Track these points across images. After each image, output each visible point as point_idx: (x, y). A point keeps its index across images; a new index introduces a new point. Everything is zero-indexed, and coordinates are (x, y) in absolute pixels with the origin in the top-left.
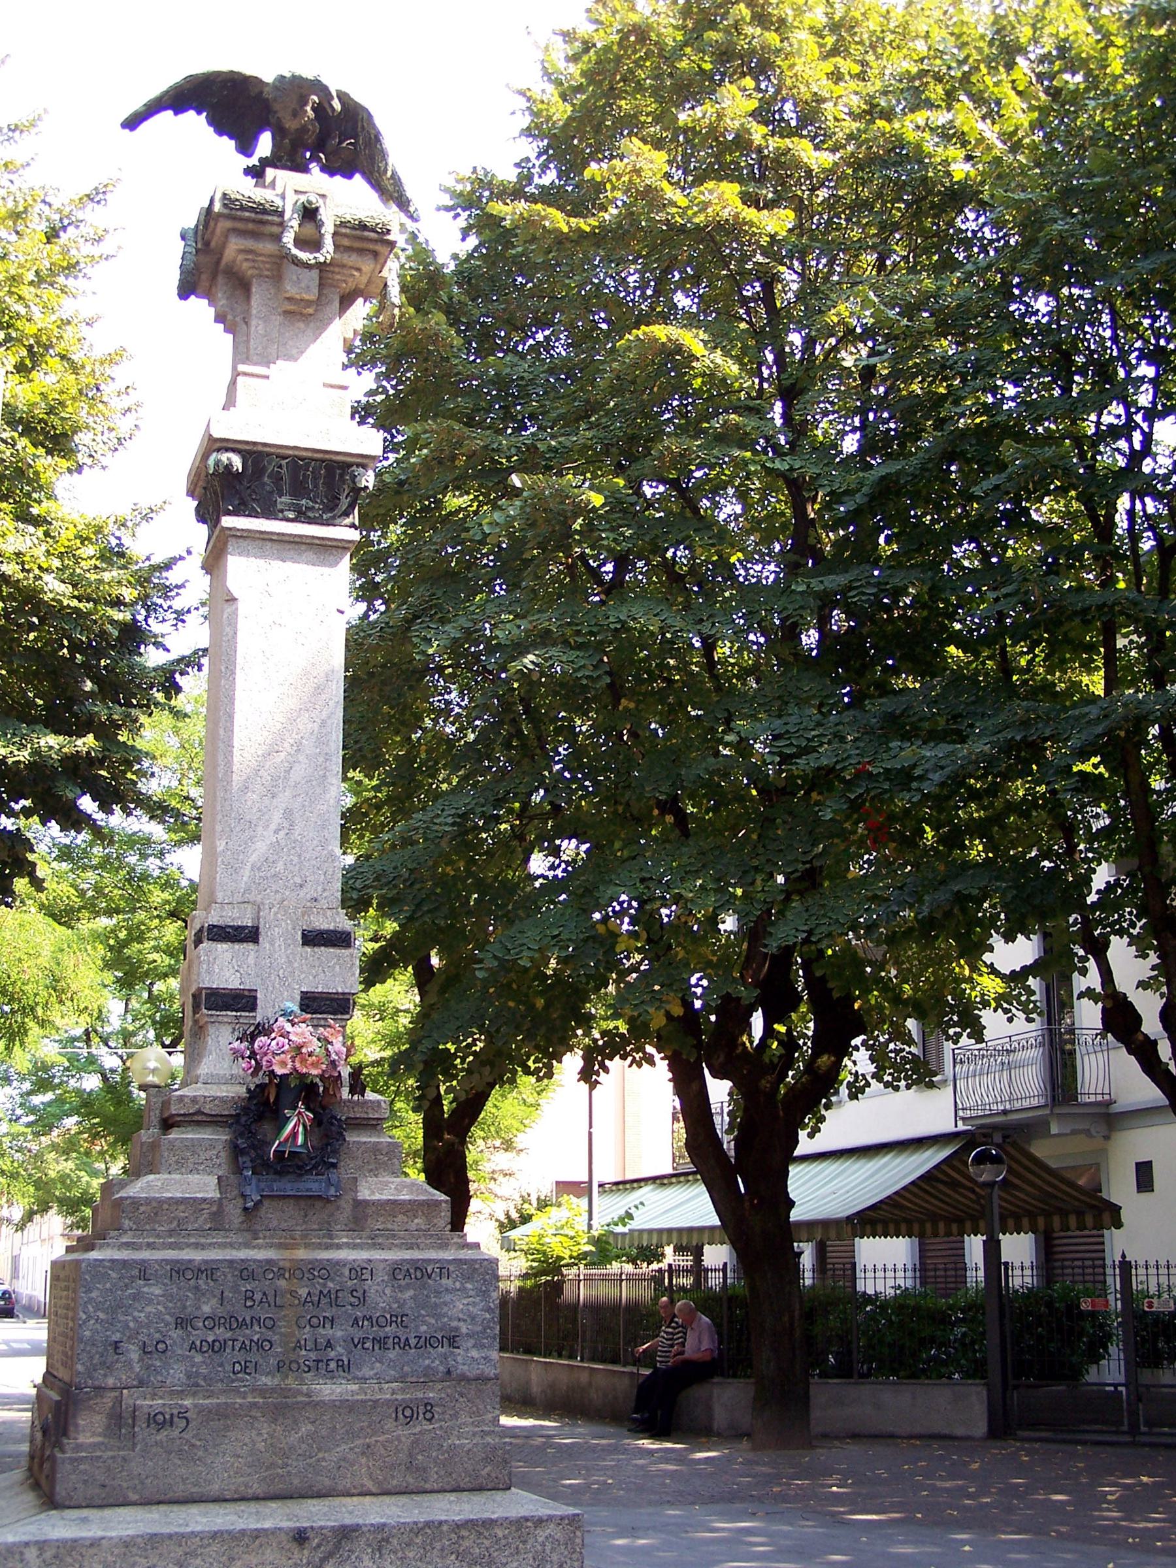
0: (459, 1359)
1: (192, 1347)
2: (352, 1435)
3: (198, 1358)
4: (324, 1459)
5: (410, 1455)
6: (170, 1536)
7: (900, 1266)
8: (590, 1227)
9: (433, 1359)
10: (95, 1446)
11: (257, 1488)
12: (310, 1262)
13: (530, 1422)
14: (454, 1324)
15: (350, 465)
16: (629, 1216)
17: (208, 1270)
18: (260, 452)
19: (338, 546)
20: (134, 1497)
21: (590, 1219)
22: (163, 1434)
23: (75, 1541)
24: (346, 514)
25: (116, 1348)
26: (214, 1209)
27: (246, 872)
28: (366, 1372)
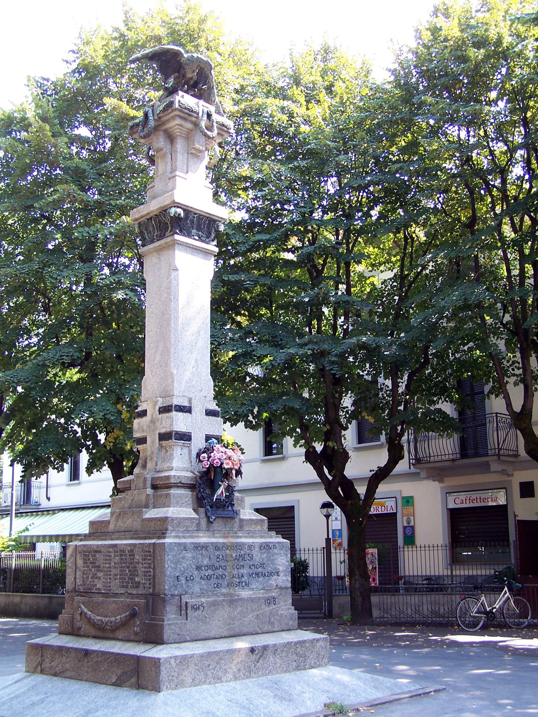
1: (201, 578)
2: (253, 611)
3: (203, 582)
6: (214, 652)
7: (440, 545)
10: (174, 618)
11: (225, 633)
12: (236, 543)
13: (8, 619)
14: (278, 567)
15: (216, 221)
16: (27, 529)
17: (205, 547)
18: (189, 210)
20: (188, 639)
21: (11, 530)
23: (186, 656)
24: (213, 241)
27: (184, 384)
28: (254, 586)
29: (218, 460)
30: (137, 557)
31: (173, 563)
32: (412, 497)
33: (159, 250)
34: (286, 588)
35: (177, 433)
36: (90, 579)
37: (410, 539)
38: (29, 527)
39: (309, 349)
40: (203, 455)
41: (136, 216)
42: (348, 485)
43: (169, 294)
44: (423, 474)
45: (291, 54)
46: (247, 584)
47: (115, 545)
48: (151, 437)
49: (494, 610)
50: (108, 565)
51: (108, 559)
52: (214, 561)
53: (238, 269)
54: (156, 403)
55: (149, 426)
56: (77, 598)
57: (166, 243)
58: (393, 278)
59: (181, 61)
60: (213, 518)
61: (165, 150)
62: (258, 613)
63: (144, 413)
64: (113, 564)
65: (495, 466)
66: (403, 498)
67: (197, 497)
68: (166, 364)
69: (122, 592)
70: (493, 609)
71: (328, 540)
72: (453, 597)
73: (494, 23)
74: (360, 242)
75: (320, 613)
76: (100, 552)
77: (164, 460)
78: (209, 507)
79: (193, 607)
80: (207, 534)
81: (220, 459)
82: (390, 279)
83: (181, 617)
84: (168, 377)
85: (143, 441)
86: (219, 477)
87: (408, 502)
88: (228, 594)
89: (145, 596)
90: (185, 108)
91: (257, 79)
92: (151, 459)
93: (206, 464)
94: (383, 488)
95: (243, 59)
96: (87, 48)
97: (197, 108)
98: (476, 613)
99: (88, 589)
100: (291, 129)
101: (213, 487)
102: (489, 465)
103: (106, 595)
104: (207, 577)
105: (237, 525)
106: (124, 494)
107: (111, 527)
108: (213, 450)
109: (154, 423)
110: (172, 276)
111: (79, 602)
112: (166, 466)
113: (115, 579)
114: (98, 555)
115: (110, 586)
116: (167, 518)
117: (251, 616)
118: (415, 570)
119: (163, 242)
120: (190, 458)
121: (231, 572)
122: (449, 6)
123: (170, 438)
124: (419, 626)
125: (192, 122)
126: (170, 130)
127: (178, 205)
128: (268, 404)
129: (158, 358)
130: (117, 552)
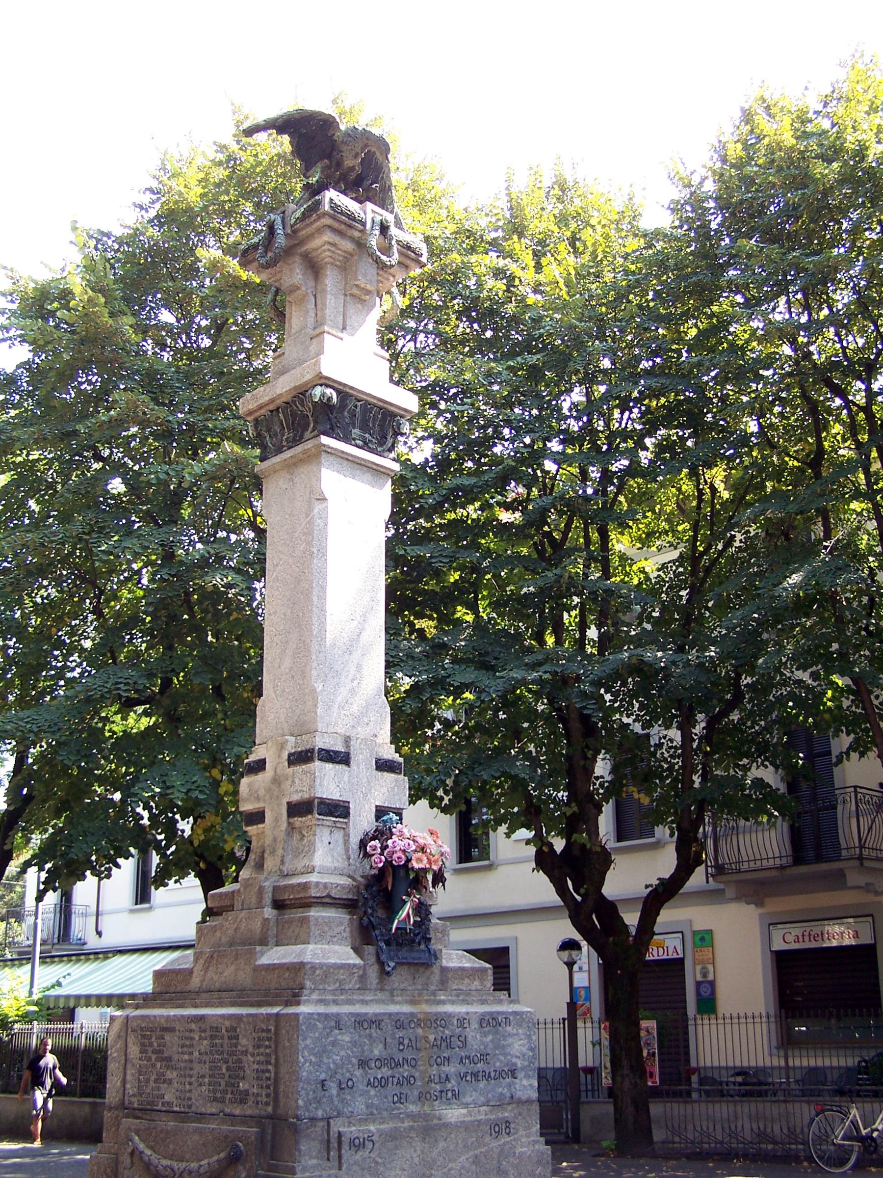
0: (517, 1086)
3: (373, 1092)
4: (452, 1169)
5: (499, 1161)
8: (31, 993)
9: (502, 1088)
10: (314, 1167)
12: (436, 1014)
14: (514, 1060)
16: (59, 984)
17: (376, 1021)
18: (347, 393)
19: (378, 471)
21: (32, 986)
22: (358, 1156)
25: (323, 1085)
26: (361, 972)
29: (400, 854)
30: (243, 1041)
31: (315, 1055)
32: (710, 932)
33: (292, 465)
34: (529, 1101)
35: (322, 801)
36: (152, 1084)
37: (708, 1004)
38: (61, 980)
39: (545, 672)
40: (373, 843)
41: (250, 407)
42: (609, 910)
43: (309, 544)
44: (730, 893)
45: (507, 189)
46: (456, 1096)
47: (202, 1018)
48: (272, 810)
49: (875, 1134)
50: (186, 1057)
51: (187, 1045)
52: (394, 1051)
53: (418, 538)
54: (282, 746)
55: (269, 790)
56: (127, 1122)
57: (305, 452)
58: (677, 560)
59: (335, 138)
60: (392, 964)
61: (303, 289)
62: (477, 1152)
63: (260, 766)
64: (196, 1054)
65: (854, 878)
66: (694, 933)
67: (361, 924)
68: (303, 672)
69: (214, 1110)
70: (873, 1131)
71: (572, 1006)
72: (790, 1106)
73: (850, 124)
74: (620, 502)
75: (560, 1133)
76: (172, 1030)
77: (297, 853)
78: (382, 944)
79: (352, 1142)
80: (380, 995)
81: (404, 851)
82: (674, 562)
83: (329, 1164)
84: (306, 697)
85: (258, 817)
86: (402, 886)
87: (702, 939)
88: (419, 1115)
89: (258, 1120)
90: (342, 213)
91: (452, 228)
92: (273, 852)
93: (378, 861)
94: (666, 916)
95: (428, 197)
96: (173, 183)
97: (362, 215)
98: (843, 1139)
99: (148, 1103)
100: (510, 305)
101: (391, 906)
102: (844, 876)
103: (182, 1116)
104: (380, 1082)
105: (436, 977)
106: (220, 918)
107: (196, 982)
108: (392, 834)
109: (279, 784)
110: (316, 510)
111: (129, 1129)
112: (300, 864)
113: (200, 1085)
114: (167, 1037)
115: (190, 1099)
116: (302, 964)
117: (463, 1158)
118: (715, 1057)
119: (298, 449)
120: (347, 850)
121: (426, 1071)
122: (772, 103)
123: (310, 812)
124: (739, 1160)
125: (352, 239)
126: (314, 254)
127: (328, 382)
128: (473, 769)
129: (287, 662)
130: (204, 1031)
